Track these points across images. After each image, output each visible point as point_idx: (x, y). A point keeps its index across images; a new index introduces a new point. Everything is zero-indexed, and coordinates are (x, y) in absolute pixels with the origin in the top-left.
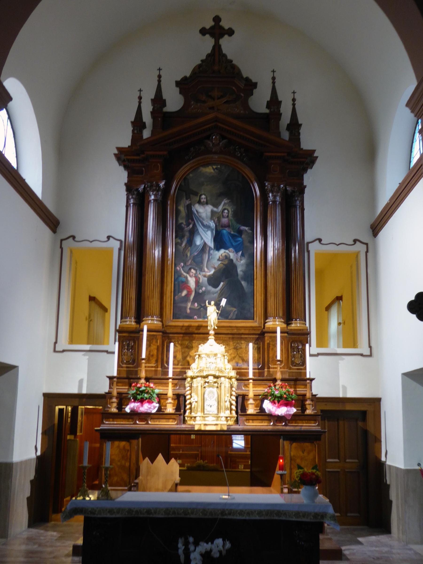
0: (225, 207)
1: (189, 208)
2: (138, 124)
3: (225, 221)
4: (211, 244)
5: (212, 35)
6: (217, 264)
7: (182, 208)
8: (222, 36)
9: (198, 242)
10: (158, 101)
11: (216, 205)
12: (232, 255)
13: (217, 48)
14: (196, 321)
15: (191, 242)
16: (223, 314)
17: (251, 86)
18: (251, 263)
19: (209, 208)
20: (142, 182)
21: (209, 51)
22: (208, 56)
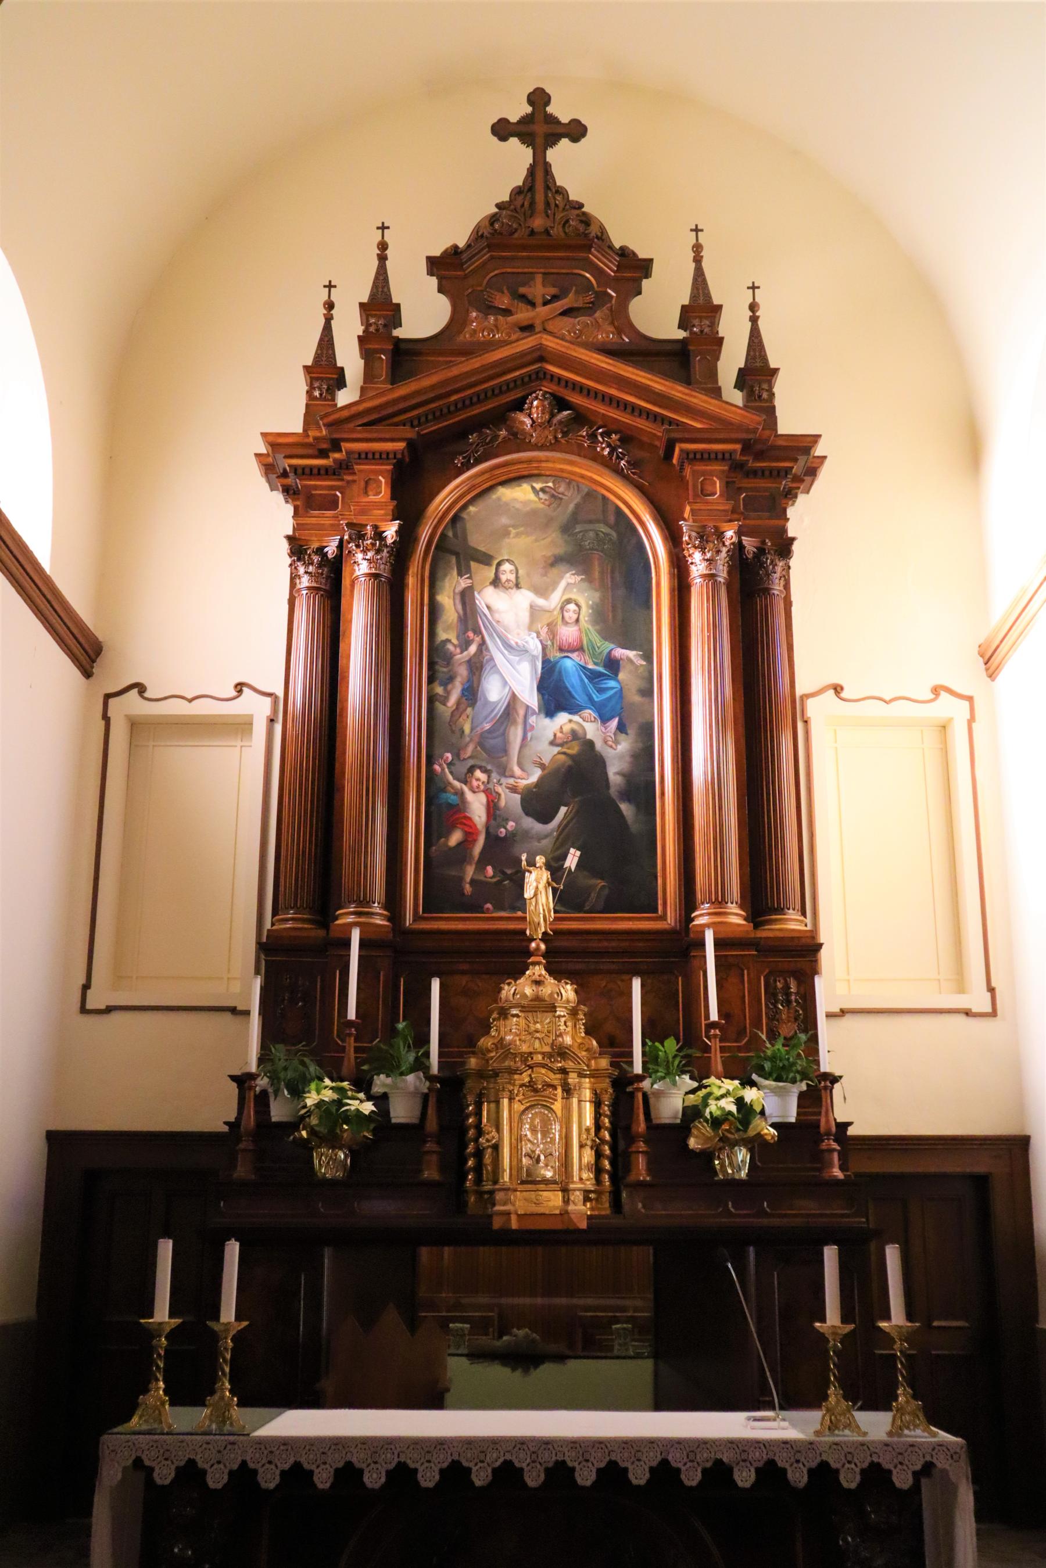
0: (573, 598)
1: (466, 597)
2: (324, 373)
3: (568, 633)
4: (530, 697)
5: (527, 138)
6: (549, 754)
7: (447, 600)
8: (552, 139)
9: (493, 691)
10: (381, 308)
11: (543, 591)
12: (592, 730)
13: (540, 172)
14: (493, 919)
15: (472, 694)
16: (568, 897)
17: (635, 269)
18: (645, 756)
19: (524, 598)
20: (336, 529)
21: (518, 179)
22: (517, 192)
